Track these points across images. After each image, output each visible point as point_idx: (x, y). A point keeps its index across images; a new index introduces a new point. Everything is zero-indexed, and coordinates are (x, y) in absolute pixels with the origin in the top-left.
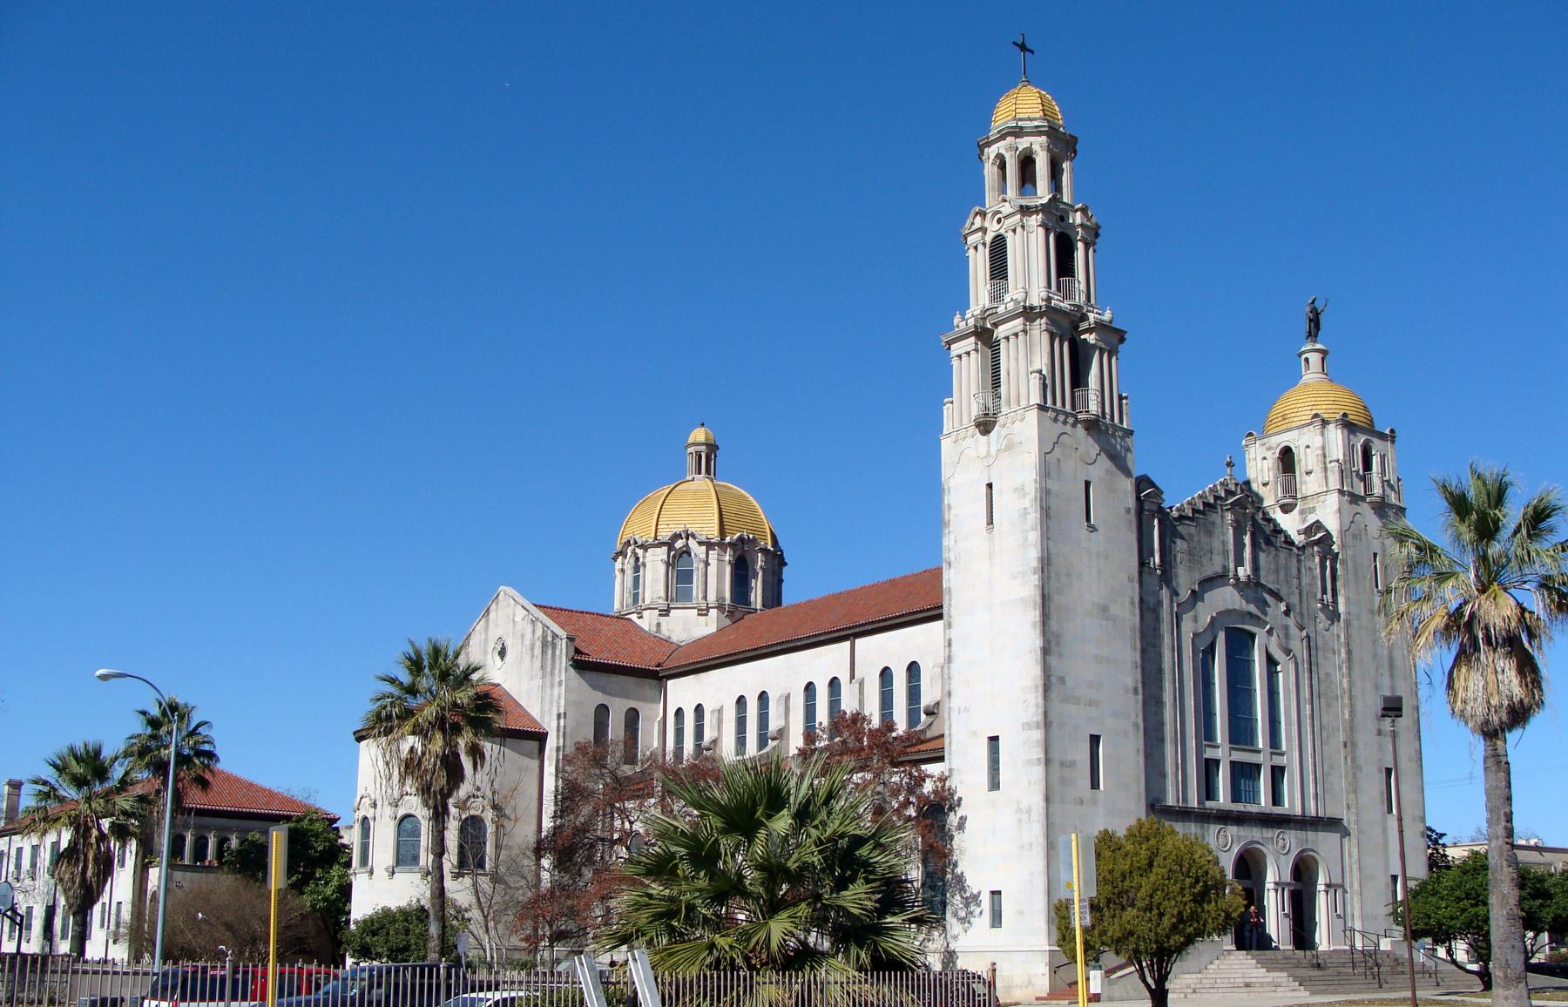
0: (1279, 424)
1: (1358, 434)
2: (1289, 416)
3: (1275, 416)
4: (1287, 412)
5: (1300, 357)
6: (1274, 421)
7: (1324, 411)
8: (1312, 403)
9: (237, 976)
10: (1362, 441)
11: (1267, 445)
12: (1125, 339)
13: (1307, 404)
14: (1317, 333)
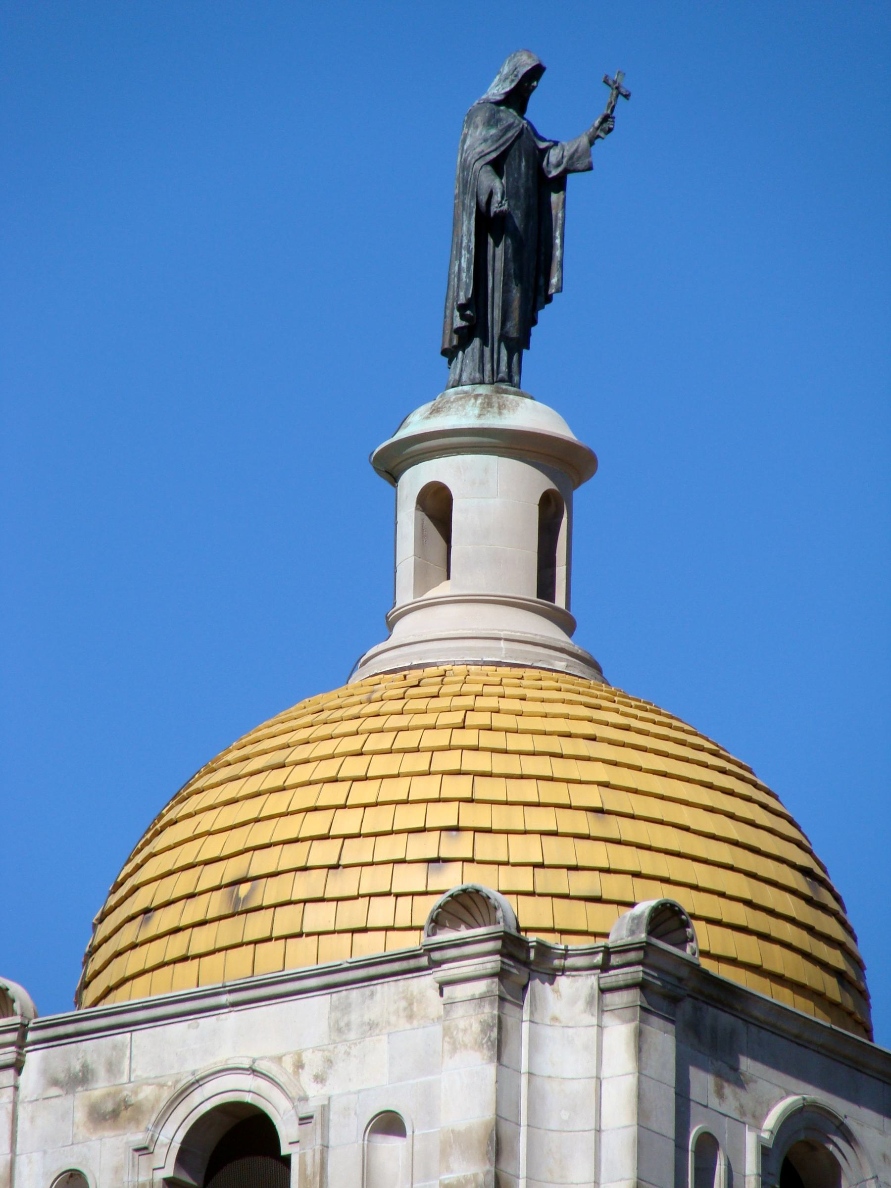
0: (202, 940)
1: (746, 1064)
2: (271, 892)
3: (182, 884)
4: (262, 863)
5: (393, 478)
6: (163, 920)
7: (523, 879)
8: (445, 815)
9: (174, 805)
10: (771, 1121)
11: (100, 1089)
12: (304, 1064)
13: (411, 817)
14: (529, 320)
